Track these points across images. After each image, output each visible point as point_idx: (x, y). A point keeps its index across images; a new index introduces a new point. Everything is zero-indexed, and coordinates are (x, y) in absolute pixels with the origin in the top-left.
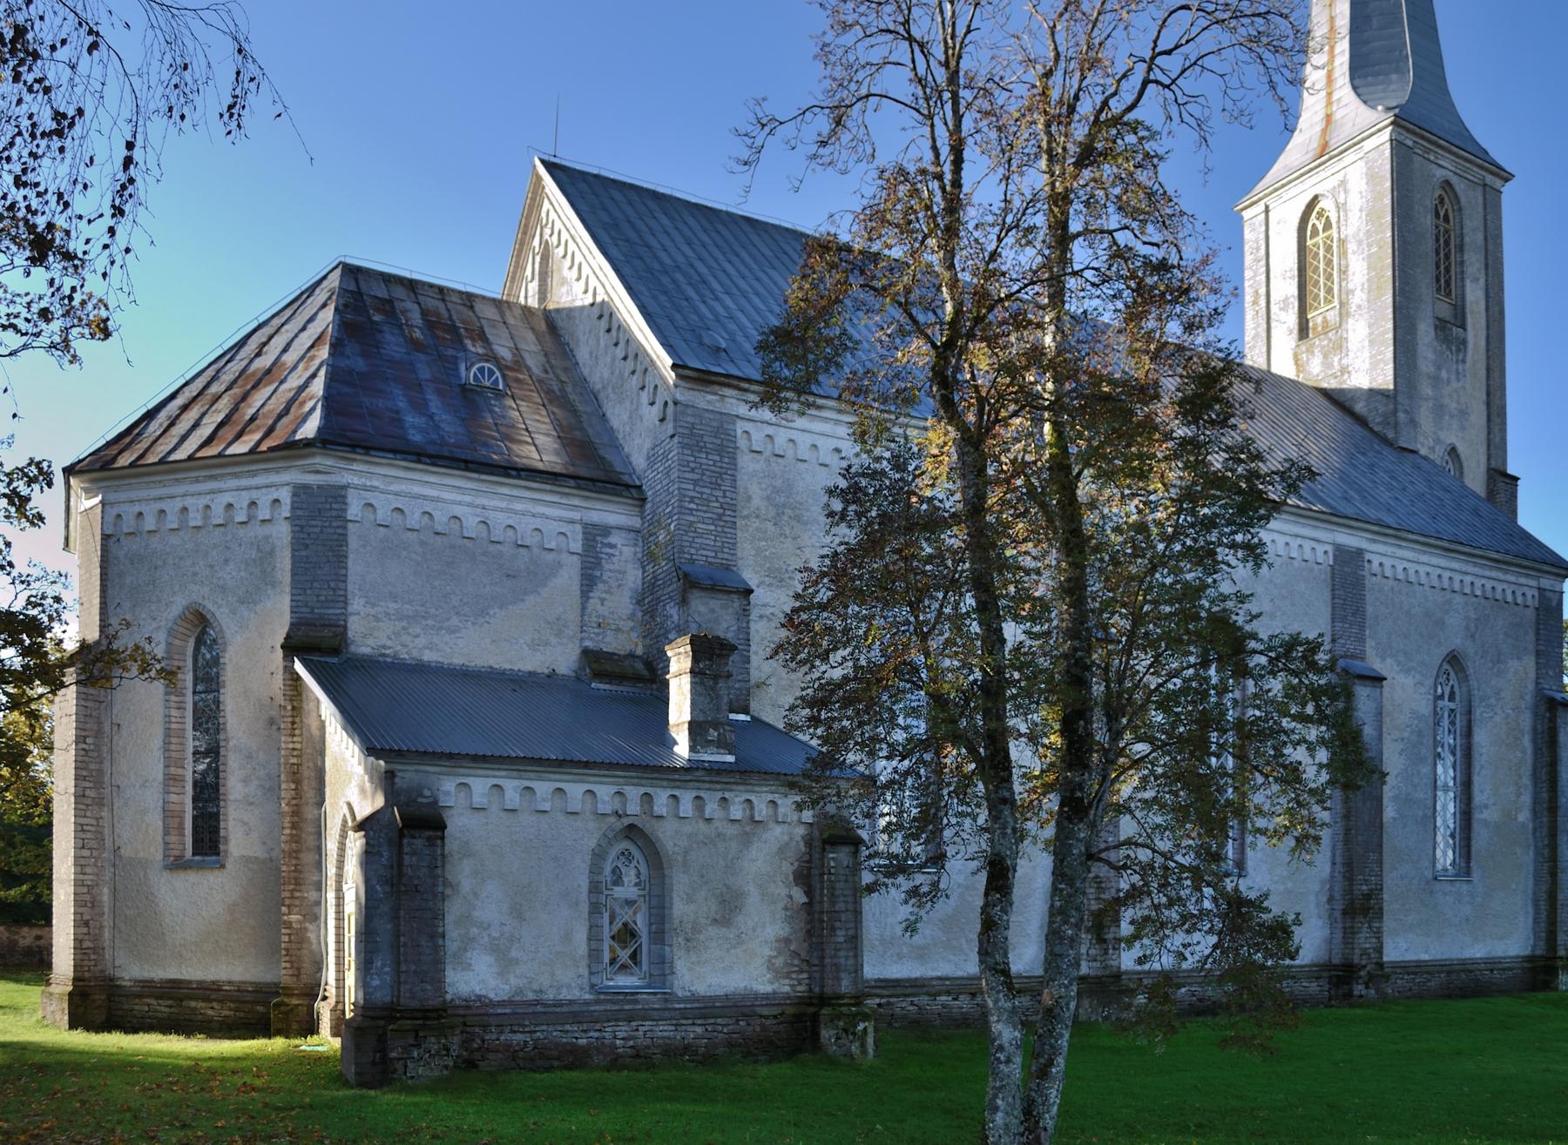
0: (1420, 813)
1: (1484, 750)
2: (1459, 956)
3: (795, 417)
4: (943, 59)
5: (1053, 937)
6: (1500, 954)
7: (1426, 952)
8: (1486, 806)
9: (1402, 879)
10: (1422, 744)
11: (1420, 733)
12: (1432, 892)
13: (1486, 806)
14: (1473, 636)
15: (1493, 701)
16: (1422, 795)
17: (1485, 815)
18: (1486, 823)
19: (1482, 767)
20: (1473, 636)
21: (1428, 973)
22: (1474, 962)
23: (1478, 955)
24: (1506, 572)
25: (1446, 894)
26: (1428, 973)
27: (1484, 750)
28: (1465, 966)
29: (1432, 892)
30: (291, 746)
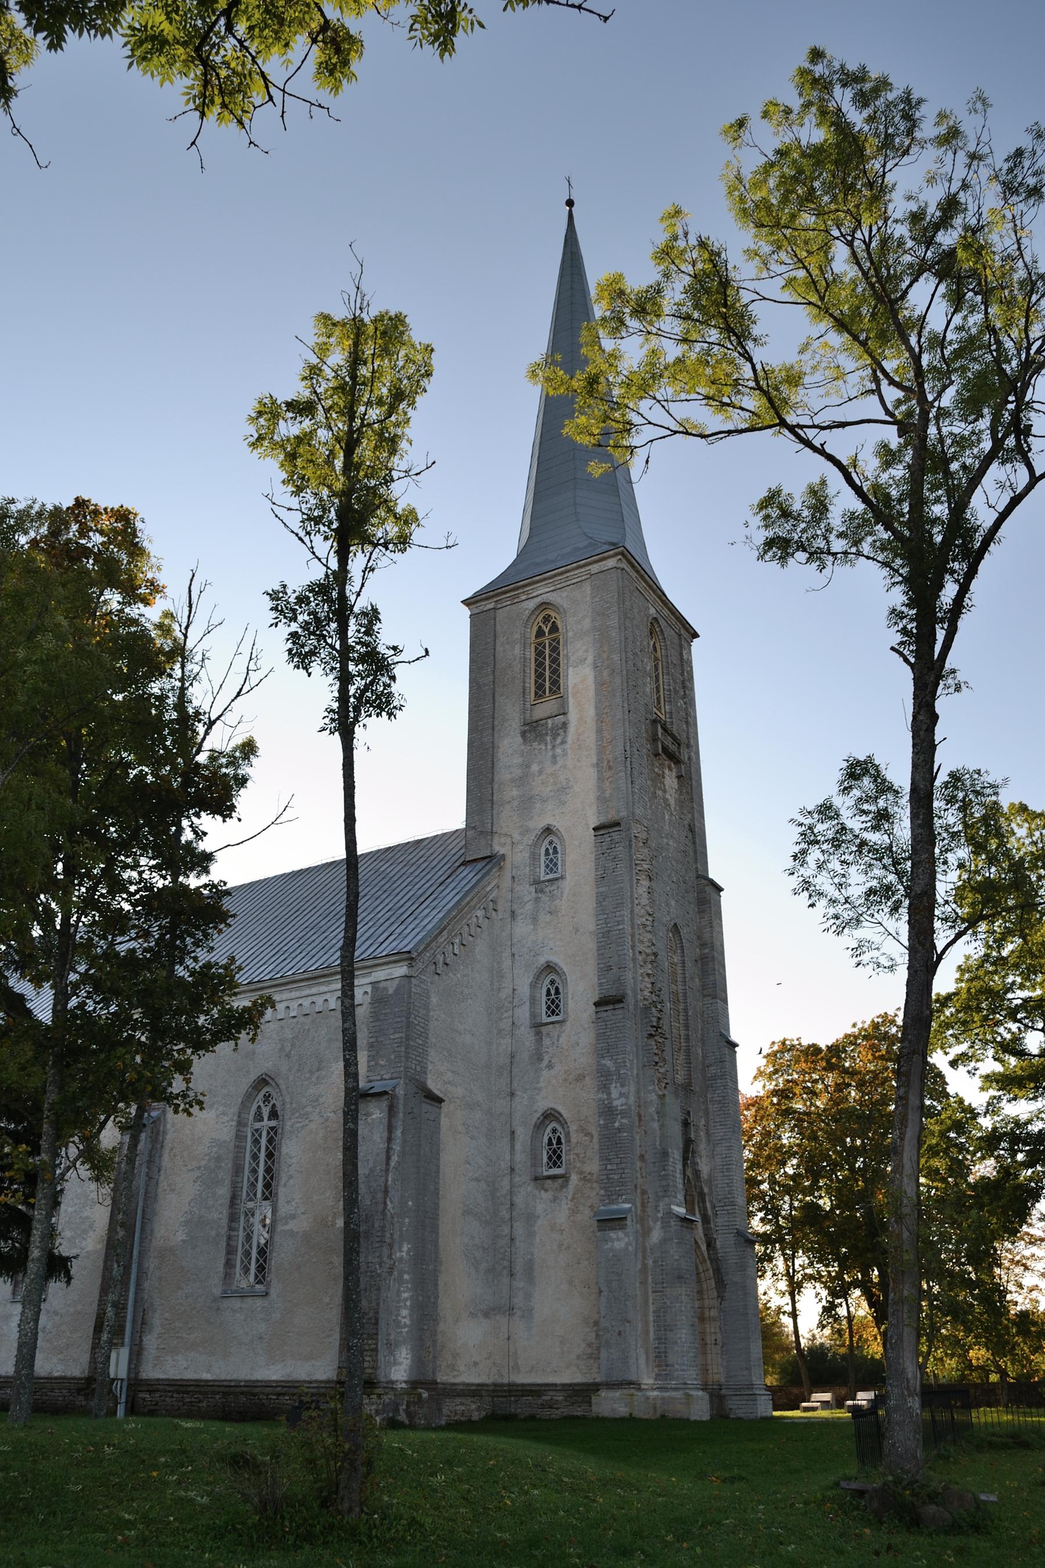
0: (213, 1233)
1: (294, 1160)
2: (249, 1378)
3: (674, 774)
4: (213, 718)
5: (109, 1357)
6: (303, 1377)
7: (208, 1371)
8: (293, 1217)
9: (187, 1297)
10: (220, 1167)
11: (219, 1159)
12: (218, 1309)
13: (293, 1217)
14: (288, 1056)
15: (309, 1109)
16: (216, 1216)
17: (292, 1225)
18: (292, 1234)
19: (291, 1177)
20: (288, 1056)
21: (200, 1393)
22: (267, 1384)
23: (274, 1378)
24: (329, 983)
25: (234, 1311)
26: (200, 1393)
27: (294, 1160)
28: (251, 1389)
29: (218, 1309)
30: (623, 1165)
